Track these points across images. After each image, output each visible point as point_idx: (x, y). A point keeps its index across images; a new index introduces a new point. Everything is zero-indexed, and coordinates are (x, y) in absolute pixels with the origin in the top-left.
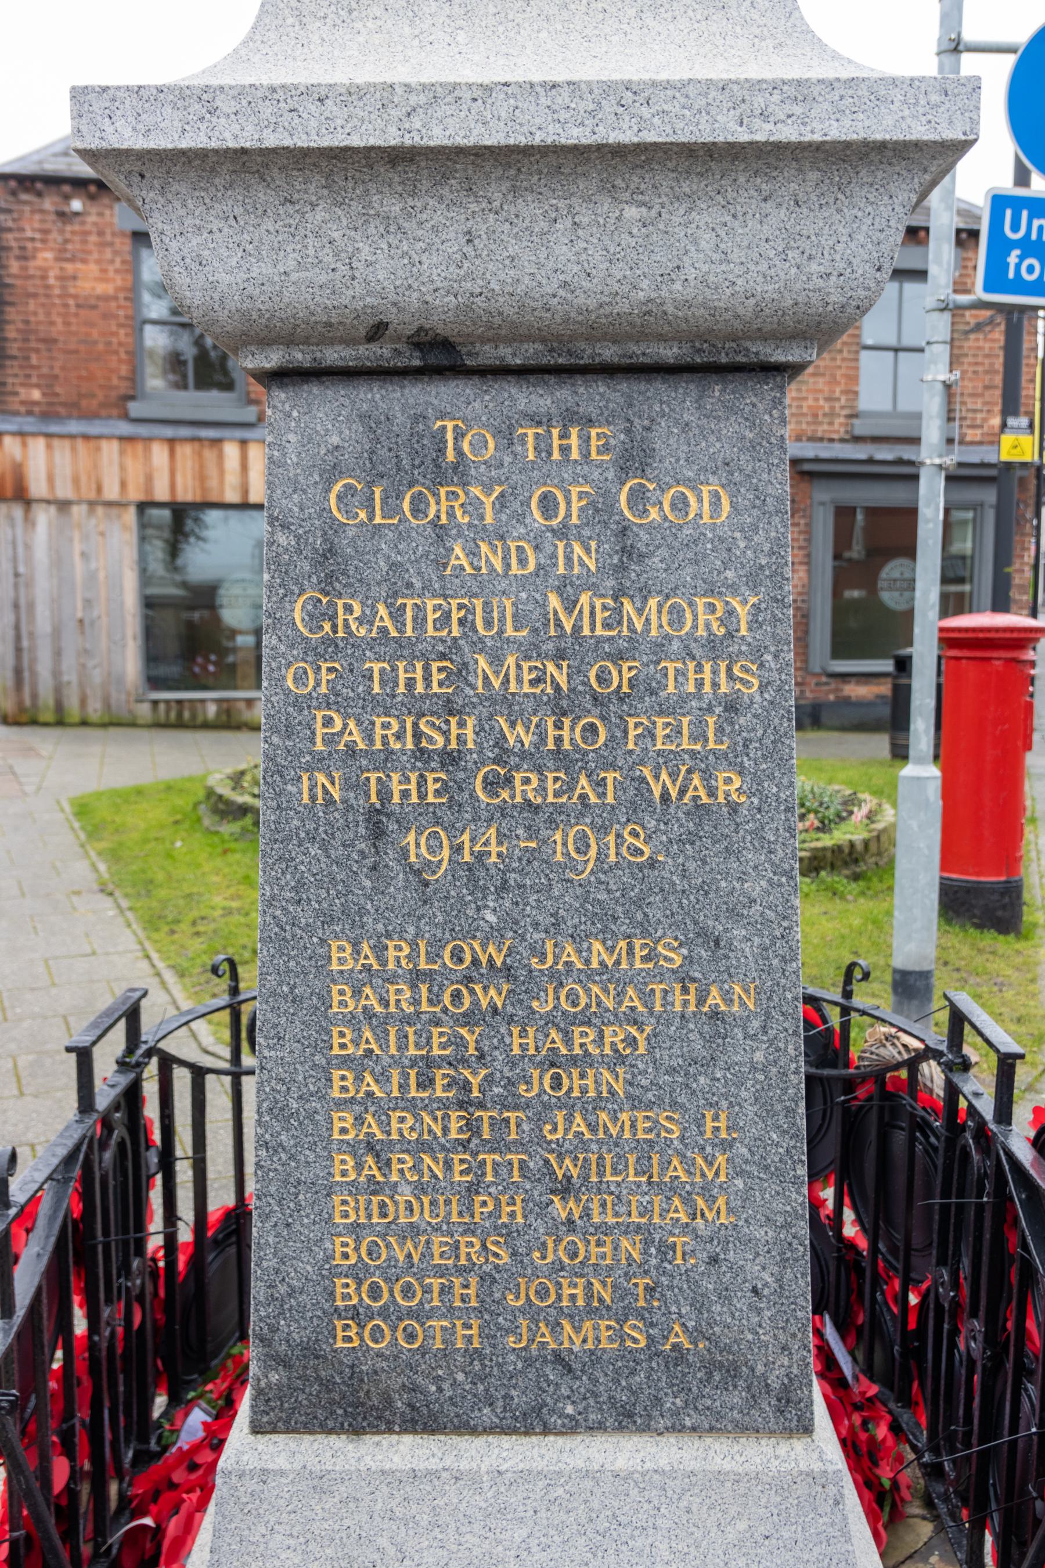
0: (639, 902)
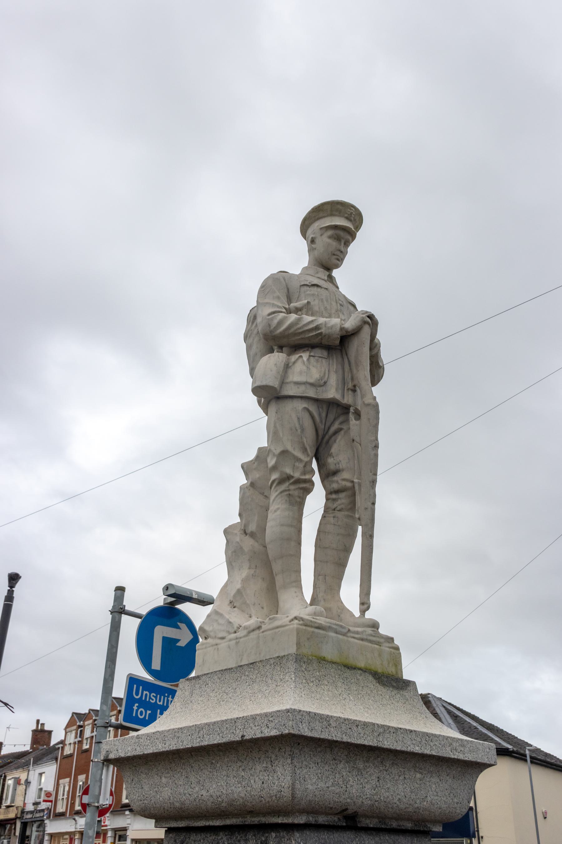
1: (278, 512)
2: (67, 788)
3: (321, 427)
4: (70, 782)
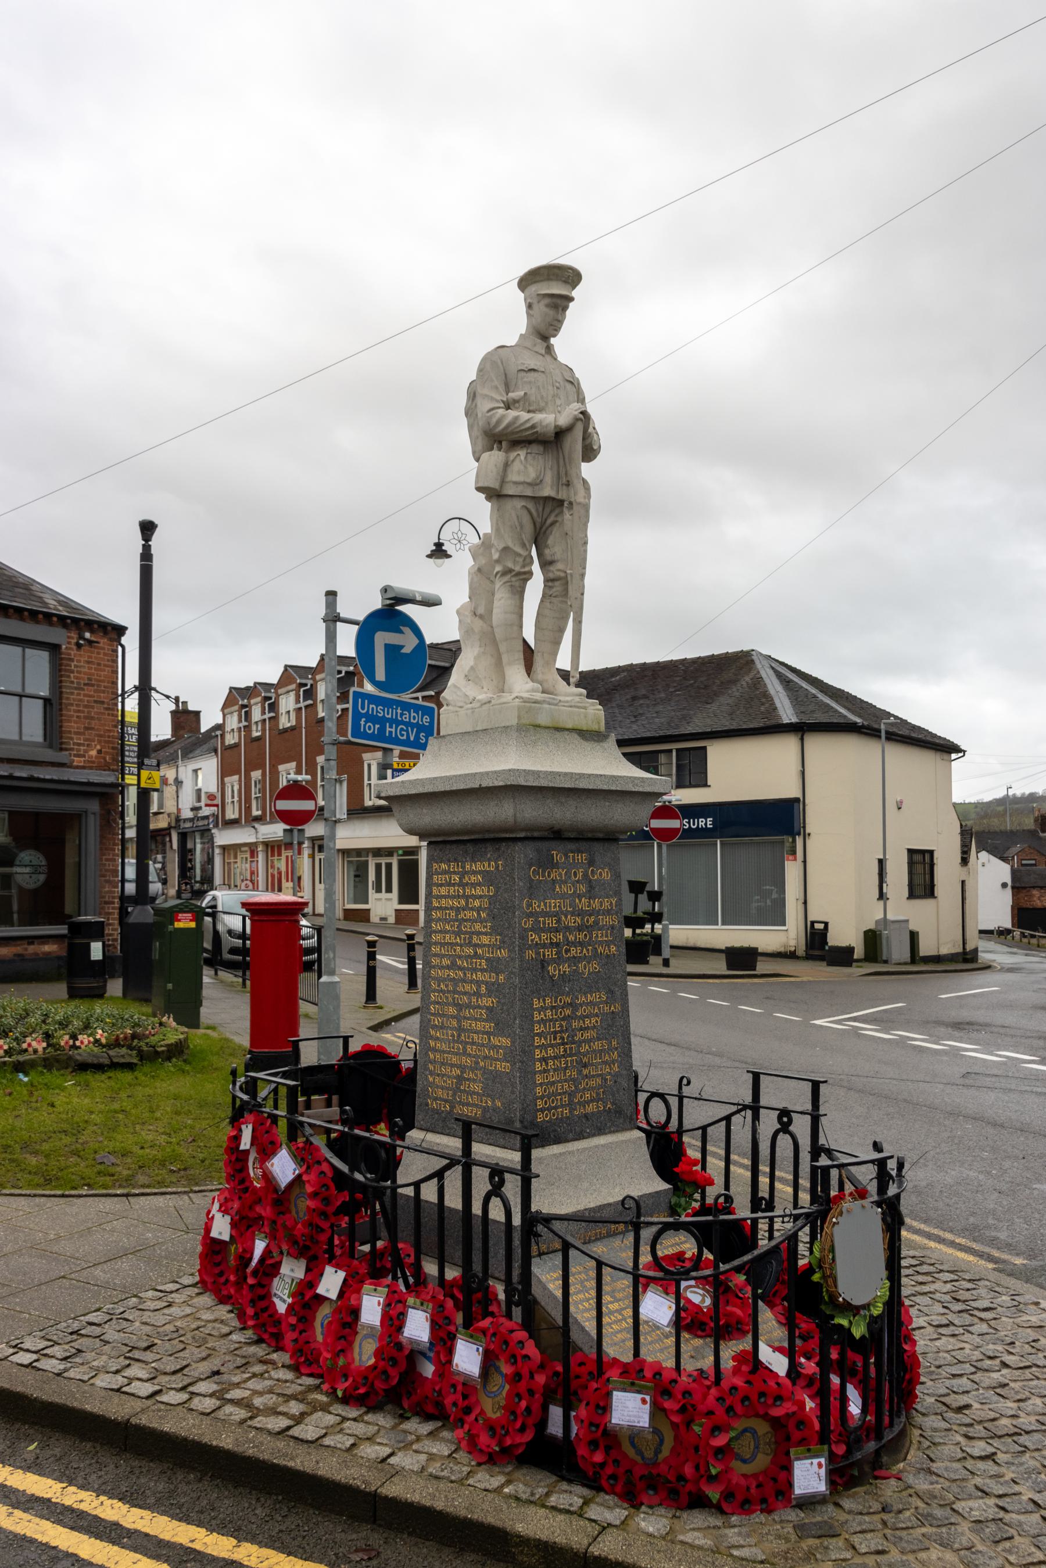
0: (597, 982)
1: (502, 601)
2: (236, 788)
3: (539, 520)
4: (240, 780)
